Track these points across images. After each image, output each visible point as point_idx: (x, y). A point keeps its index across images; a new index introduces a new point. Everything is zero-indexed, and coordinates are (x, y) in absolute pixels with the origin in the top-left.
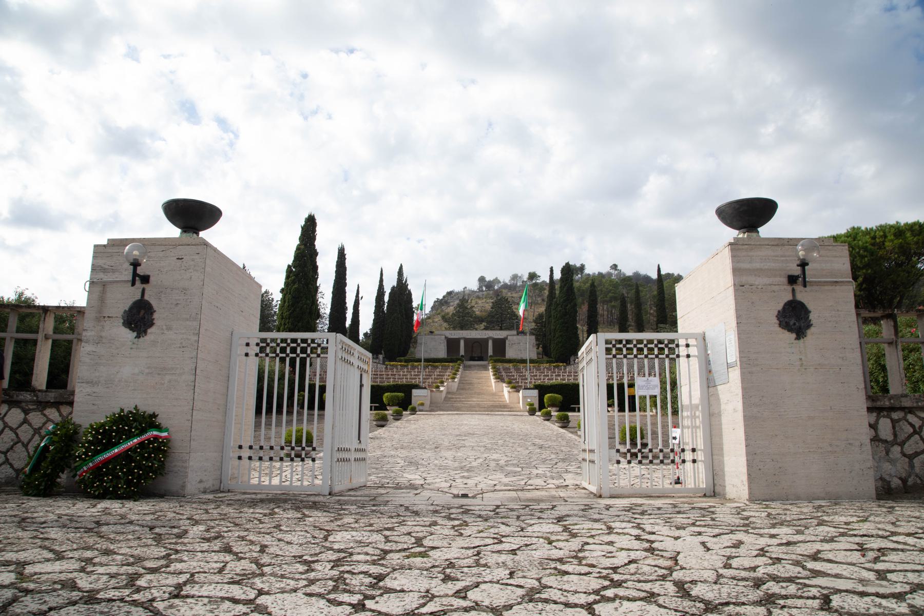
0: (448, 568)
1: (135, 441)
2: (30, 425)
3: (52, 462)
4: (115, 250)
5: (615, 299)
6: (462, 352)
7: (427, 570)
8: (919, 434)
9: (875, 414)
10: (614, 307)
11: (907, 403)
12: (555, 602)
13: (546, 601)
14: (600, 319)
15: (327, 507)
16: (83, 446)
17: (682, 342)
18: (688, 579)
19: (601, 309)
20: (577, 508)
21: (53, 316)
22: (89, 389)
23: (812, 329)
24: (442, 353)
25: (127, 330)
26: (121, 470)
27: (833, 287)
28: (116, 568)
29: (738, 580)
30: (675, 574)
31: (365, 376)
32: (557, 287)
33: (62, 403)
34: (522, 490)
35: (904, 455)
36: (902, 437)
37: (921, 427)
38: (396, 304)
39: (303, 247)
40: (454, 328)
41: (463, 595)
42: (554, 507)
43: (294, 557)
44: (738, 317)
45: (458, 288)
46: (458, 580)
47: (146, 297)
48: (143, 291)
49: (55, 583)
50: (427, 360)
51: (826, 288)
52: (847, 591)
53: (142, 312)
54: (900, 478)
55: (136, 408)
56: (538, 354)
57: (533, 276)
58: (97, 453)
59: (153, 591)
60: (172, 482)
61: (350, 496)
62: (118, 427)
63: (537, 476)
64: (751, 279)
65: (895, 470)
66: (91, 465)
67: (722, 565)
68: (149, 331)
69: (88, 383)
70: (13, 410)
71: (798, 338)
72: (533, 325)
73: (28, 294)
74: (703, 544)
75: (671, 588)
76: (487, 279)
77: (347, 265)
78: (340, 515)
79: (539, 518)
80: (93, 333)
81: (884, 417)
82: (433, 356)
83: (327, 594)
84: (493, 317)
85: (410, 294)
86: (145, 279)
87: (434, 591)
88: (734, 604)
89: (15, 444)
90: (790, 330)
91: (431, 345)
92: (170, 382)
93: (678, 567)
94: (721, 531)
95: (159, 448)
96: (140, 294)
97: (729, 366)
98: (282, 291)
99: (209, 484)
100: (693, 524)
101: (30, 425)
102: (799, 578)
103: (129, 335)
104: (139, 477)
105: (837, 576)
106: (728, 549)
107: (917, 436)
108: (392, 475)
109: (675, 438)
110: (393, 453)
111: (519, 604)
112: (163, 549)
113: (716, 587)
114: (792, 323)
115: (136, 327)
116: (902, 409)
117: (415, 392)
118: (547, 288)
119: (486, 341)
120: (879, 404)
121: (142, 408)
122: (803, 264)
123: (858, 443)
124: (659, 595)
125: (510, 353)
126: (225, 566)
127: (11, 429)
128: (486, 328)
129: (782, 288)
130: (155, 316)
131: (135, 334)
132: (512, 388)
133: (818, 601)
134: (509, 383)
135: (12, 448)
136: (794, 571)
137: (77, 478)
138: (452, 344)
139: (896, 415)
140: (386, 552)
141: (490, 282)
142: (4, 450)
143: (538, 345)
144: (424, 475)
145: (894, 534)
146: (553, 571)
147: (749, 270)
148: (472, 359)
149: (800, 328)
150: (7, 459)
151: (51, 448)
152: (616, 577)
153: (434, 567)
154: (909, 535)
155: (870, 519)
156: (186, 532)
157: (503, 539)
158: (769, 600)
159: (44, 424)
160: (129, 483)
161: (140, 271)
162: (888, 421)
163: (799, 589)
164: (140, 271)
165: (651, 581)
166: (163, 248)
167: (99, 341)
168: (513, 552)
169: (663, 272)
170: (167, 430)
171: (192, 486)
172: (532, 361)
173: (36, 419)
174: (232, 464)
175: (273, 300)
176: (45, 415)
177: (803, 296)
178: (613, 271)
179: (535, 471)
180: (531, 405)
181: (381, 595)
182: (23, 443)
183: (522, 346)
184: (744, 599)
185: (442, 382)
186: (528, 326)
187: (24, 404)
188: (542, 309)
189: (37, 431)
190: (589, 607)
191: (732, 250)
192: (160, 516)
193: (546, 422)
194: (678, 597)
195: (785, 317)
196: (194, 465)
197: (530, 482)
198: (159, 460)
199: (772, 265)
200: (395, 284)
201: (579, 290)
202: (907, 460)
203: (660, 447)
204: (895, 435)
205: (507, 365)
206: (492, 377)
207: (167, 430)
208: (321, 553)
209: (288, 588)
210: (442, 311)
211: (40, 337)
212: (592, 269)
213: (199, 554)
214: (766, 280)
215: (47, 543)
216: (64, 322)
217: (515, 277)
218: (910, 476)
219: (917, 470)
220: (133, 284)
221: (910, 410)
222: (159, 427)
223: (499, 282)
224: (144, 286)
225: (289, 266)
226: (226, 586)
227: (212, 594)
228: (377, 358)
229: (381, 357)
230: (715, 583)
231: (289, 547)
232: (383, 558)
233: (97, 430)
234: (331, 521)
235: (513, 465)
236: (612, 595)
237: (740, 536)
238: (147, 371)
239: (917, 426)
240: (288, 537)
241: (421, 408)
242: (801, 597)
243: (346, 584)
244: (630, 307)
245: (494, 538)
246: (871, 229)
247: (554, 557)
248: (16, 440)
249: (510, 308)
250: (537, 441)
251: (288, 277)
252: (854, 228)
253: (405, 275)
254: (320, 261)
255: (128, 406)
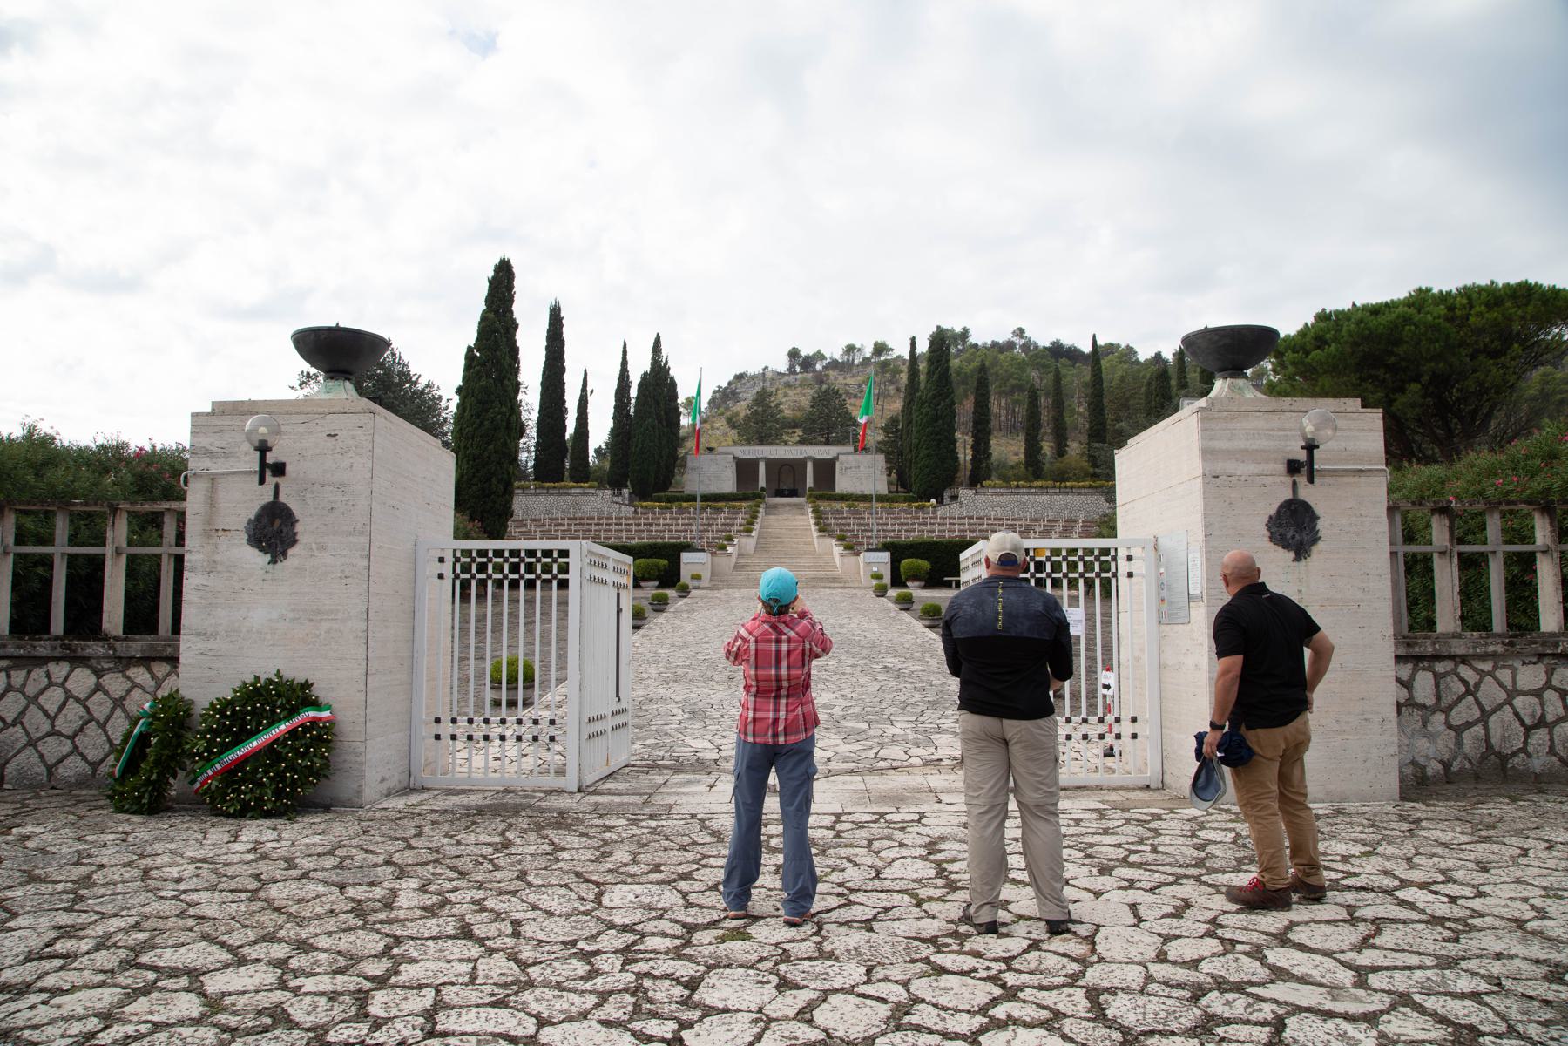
0: (783, 961)
1: (283, 727)
2: (106, 693)
3: (157, 763)
4: (227, 421)
5: (1020, 388)
6: (762, 483)
7: (752, 967)
8: (1473, 694)
9: (1410, 666)
10: (1017, 402)
11: (1459, 648)
12: (930, 1031)
13: (918, 1028)
14: (993, 423)
15: (582, 822)
16: (204, 737)
17: (1122, 553)
18: (1106, 984)
19: (997, 405)
20: (955, 820)
21: (125, 515)
22: (202, 645)
23: (1320, 545)
24: (728, 484)
25: (256, 551)
26: (266, 773)
27: (1356, 479)
28: (326, 979)
29: (1172, 987)
30: (1090, 972)
31: (623, 593)
32: (922, 366)
33: (154, 659)
34: (871, 771)
35: (1450, 727)
36: (1447, 700)
37: (1477, 685)
38: (651, 403)
39: (492, 315)
40: (749, 442)
41: (807, 1016)
42: (922, 816)
43: (563, 943)
44: (1207, 526)
45: (754, 369)
46: (798, 987)
47: (282, 498)
48: (277, 487)
49: (260, 1013)
50: (706, 498)
51: (1346, 479)
52: (1309, 1010)
53: (278, 522)
54: (1442, 762)
55: (278, 674)
56: (890, 483)
57: (880, 349)
58: (226, 748)
59: (399, 1026)
60: (342, 786)
61: (610, 793)
62: (254, 707)
63: (894, 740)
64: (1231, 466)
65: (1432, 749)
66: (218, 766)
67: (1154, 955)
68: (290, 552)
69: (199, 634)
70: (78, 671)
71: (1298, 559)
72: (881, 437)
73: (44, 428)
74: (1133, 907)
75: (1082, 1003)
76: (803, 353)
77: (565, 336)
78: (606, 843)
79: (901, 845)
80: (200, 556)
81: (1424, 669)
82: (714, 489)
83: (631, 1020)
84: (814, 421)
85: (673, 385)
86: (279, 469)
87: (768, 1010)
88: (1160, 1033)
89: (88, 722)
90: (1286, 547)
91: (711, 472)
92: (328, 632)
93: (1095, 958)
94: (1163, 878)
95: (319, 737)
96: (271, 493)
97: (1190, 598)
98: (459, 391)
99: (394, 781)
100: (1124, 862)
101: (106, 693)
102: (1252, 984)
103: (260, 559)
104: (294, 783)
105: (1304, 980)
106: (1168, 920)
107: (1470, 698)
108: (668, 740)
109: (1107, 687)
110: (662, 691)
111: (883, 1033)
112: (378, 937)
113: (1141, 1000)
114: (1289, 535)
115: (269, 545)
116: (1452, 657)
117: (686, 557)
118: (905, 368)
119: (801, 463)
120: (1417, 650)
121: (288, 674)
122: (1310, 447)
123: (1377, 719)
124: (1065, 1016)
125: (843, 484)
126: (474, 968)
127: (78, 700)
128: (802, 442)
129: (1278, 479)
130: (299, 528)
131: (268, 557)
132: (846, 548)
133: (1267, 1029)
134: (841, 539)
135: (81, 729)
136: (1250, 968)
137: (198, 785)
138: (745, 469)
139: (1440, 667)
140: (691, 929)
141: (807, 357)
142: (70, 733)
143: (889, 471)
144: (718, 741)
145: (1405, 883)
146: (925, 968)
147: (1228, 451)
148: (780, 493)
149: (1301, 543)
150: (76, 748)
151: (154, 740)
152: (1011, 979)
153: (762, 959)
154: (1423, 886)
155: (1380, 849)
156: (394, 893)
157: (852, 897)
158: (1206, 1026)
159: (129, 691)
160: (279, 793)
161: (271, 458)
162: (1430, 675)
163: (1249, 1005)
164: (271, 458)
165: (1056, 987)
166: (303, 418)
167: (211, 568)
168: (868, 925)
169: (1100, 342)
170: (329, 708)
171: (370, 791)
172: (880, 498)
173: (115, 683)
174: (425, 748)
175: (440, 398)
176: (128, 678)
177: (1307, 493)
178: (1017, 340)
179: (890, 730)
180: (878, 576)
181: (700, 1020)
182: (98, 722)
183: (862, 473)
184: (1173, 1026)
185: (730, 539)
186: (875, 437)
187: (93, 662)
188: (897, 405)
189: (118, 703)
190: (973, 1038)
191: (1202, 420)
192: (343, 858)
193: (904, 614)
194: (1089, 1020)
195: (1280, 525)
196: (371, 758)
197: (883, 753)
198: (323, 757)
199: (1265, 444)
200: (648, 368)
201: (958, 374)
202: (1453, 734)
203: (1084, 715)
204: (1438, 697)
205: (838, 505)
206: (813, 528)
207: (329, 708)
208: (599, 934)
209: (575, 1010)
210: (727, 409)
211: (108, 551)
212: (981, 335)
213: (430, 943)
214: (1253, 468)
215: (207, 928)
216: (107, 471)
217: (850, 349)
218: (1455, 758)
219: (1467, 749)
220: (262, 481)
221: (1464, 659)
222: (316, 704)
223: (823, 357)
224: (277, 479)
225: (469, 349)
226: (491, 1010)
227: (477, 1027)
228: (620, 494)
229: (626, 492)
230: (1142, 992)
231: (549, 923)
232: (688, 943)
233: (222, 712)
234: (597, 859)
235: (855, 716)
236: (1003, 1017)
237: (1188, 890)
238: (291, 615)
239: (1472, 683)
240: (545, 901)
241: (696, 583)
242: (1248, 1022)
243: (650, 1001)
244: (1044, 402)
245: (839, 895)
246: (1449, 293)
247: (925, 935)
248: (87, 717)
249: (843, 405)
250: (892, 661)
251: (468, 368)
252: (1420, 290)
253: (664, 354)
254: (521, 338)
255: (267, 671)
